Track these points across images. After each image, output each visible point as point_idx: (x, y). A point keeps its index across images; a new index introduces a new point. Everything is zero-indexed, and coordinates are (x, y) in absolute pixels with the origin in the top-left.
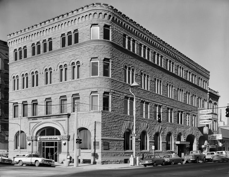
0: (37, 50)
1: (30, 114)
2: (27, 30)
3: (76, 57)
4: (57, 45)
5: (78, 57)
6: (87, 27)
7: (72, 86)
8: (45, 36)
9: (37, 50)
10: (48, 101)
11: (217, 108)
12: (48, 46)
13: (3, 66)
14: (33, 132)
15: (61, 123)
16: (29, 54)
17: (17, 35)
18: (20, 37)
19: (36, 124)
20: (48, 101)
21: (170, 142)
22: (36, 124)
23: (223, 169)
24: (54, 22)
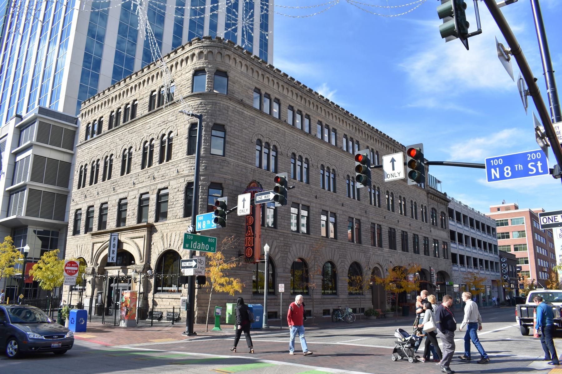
0: (114, 121)
1: (95, 229)
2: (106, 92)
3: (168, 124)
4: (141, 111)
5: (171, 124)
6: (187, 74)
7: (159, 174)
8: (128, 99)
9: (114, 121)
10: (122, 207)
11: (115, 323)
12: (130, 113)
13: (66, 213)
14: (97, 260)
15: (137, 242)
16: (105, 127)
17: (94, 101)
18: (96, 104)
19: (101, 244)
20: (122, 207)
21: (198, 314)
22: (101, 244)
23: (120, 347)
24: (143, 74)
